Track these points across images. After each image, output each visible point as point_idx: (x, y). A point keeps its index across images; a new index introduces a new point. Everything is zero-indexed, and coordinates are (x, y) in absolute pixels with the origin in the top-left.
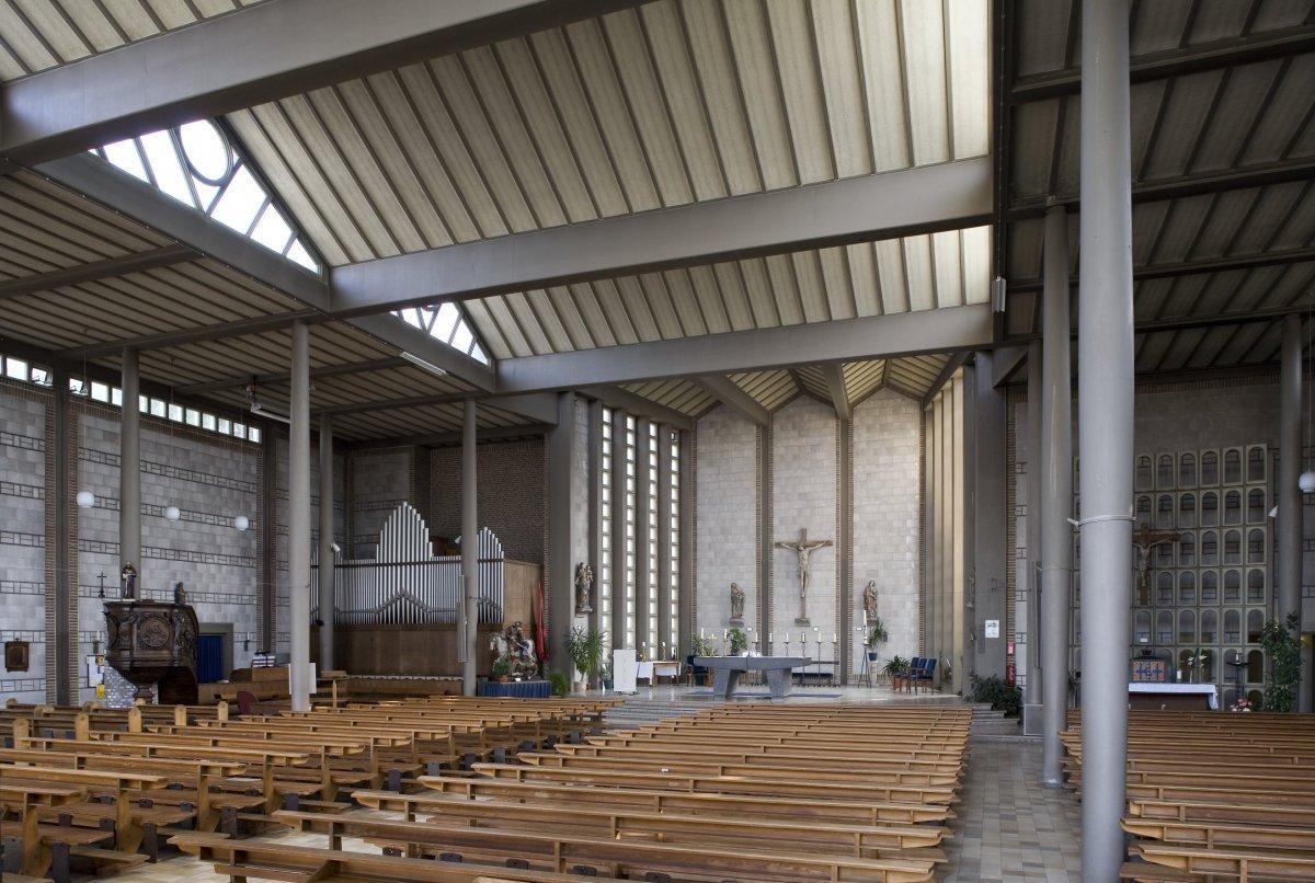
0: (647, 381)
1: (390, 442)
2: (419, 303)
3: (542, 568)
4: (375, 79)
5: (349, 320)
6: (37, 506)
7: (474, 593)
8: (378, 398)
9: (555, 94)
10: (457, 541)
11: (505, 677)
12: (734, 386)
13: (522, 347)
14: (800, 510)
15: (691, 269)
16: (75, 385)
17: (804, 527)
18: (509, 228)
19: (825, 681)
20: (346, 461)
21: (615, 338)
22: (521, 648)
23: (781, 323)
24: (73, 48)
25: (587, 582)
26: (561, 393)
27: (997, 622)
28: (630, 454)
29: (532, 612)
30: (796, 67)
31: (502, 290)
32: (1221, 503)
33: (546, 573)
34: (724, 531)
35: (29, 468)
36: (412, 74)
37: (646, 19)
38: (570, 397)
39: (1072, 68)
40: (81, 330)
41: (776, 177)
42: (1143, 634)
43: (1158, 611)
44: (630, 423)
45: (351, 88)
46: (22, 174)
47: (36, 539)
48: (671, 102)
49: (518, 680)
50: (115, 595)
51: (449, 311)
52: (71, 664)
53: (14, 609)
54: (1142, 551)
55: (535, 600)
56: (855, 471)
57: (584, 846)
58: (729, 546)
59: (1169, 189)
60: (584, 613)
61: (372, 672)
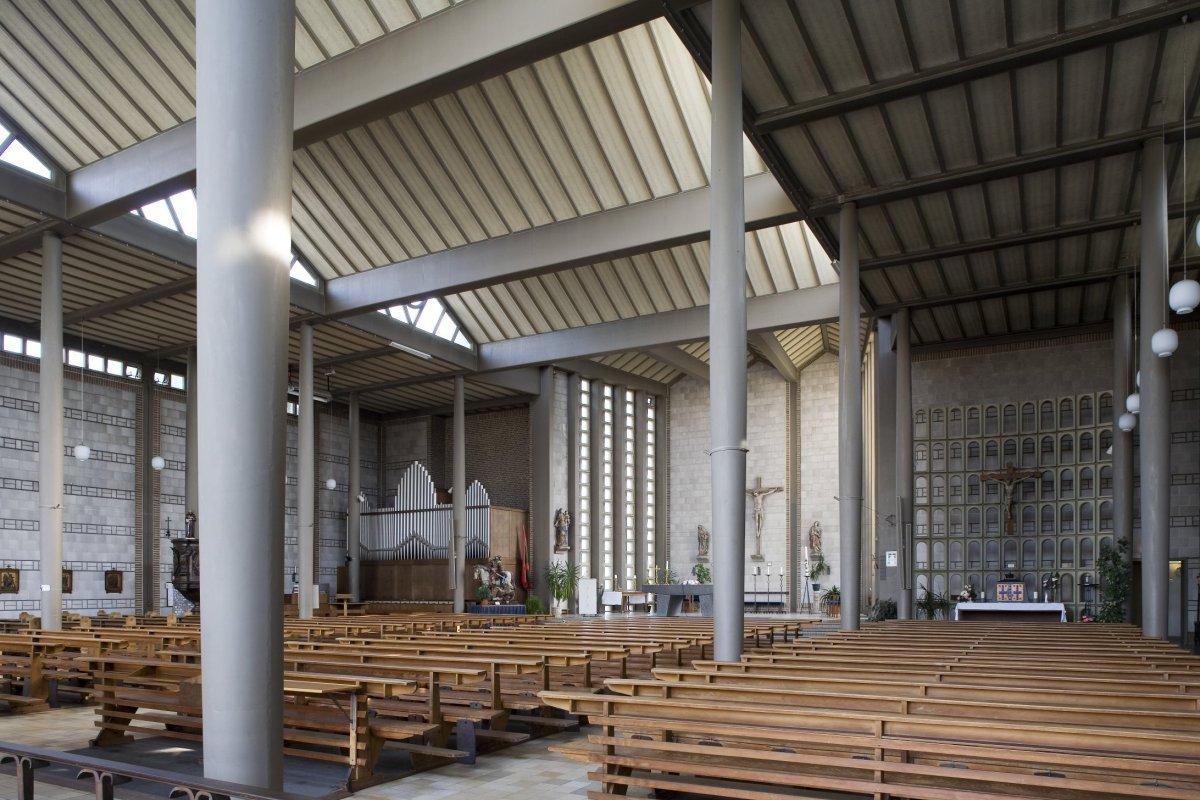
0: (623, 352)
1: (411, 413)
2: (405, 301)
3: (527, 513)
4: (372, 125)
5: (344, 320)
6: (130, 469)
7: (462, 533)
9: (461, 144)
10: (450, 491)
12: (690, 357)
13: (496, 334)
14: (756, 461)
15: (559, 273)
16: (159, 377)
19: (777, 609)
21: (534, 329)
22: (501, 576)
23: (694, 304)
24: (145, 130)
25: (565, 525)
26: (542, 367)
28: (608, 417)
29: (518, 547)
31: (472, 286)
32: (1076, 446)
36: (378, 127)
37: (514, 84)
38: (549, 371)
39: (1014, 46)
40: (156, 336)
42: (1011, 562)
44: (607, 391)
45: (336, 141)
46: (85, 233)
50: (181, 536)
51: (434, 306)
52: (155, 589)
53: (112, 546)
54: (1007, 487)
55: (520, 539)
57: (315, 664)
60: (564, 550)
61: (391, 599)
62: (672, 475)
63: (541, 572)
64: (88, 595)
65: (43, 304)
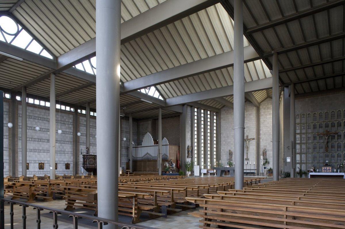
1: (146, 119)
2: (145, 87)
6: (71, 136)
8: (141, 109)
11: (168, 172)
16: (79, 111)
17: (248, 135)
18: (157, 71)
20: (138, 124)
22: (172, 165)
23: (228, 85)
26: (183, 105)
27: (290, 157)
30: (209, 30)
31: (164, 83)
33: (180, 148)
34: (228, 137)
35: (70, 128)
36: (132, 42)
38: (186, 106)
41: (211, 54)
42: (327, 160)
43: (331, 153)
44: (202, 111)
46: (61, 73)
47: (71, 142)
48: (184, 41)
49: (171, 172)
51: (153, 88)
54: (326, 137)
56: (261, 120)
58: (229, 140)
59: (332, 38)
60: (190, 157)
62: (221, 135)
63: (183, 163)
64: (61, 170)
65: (51, 93)
